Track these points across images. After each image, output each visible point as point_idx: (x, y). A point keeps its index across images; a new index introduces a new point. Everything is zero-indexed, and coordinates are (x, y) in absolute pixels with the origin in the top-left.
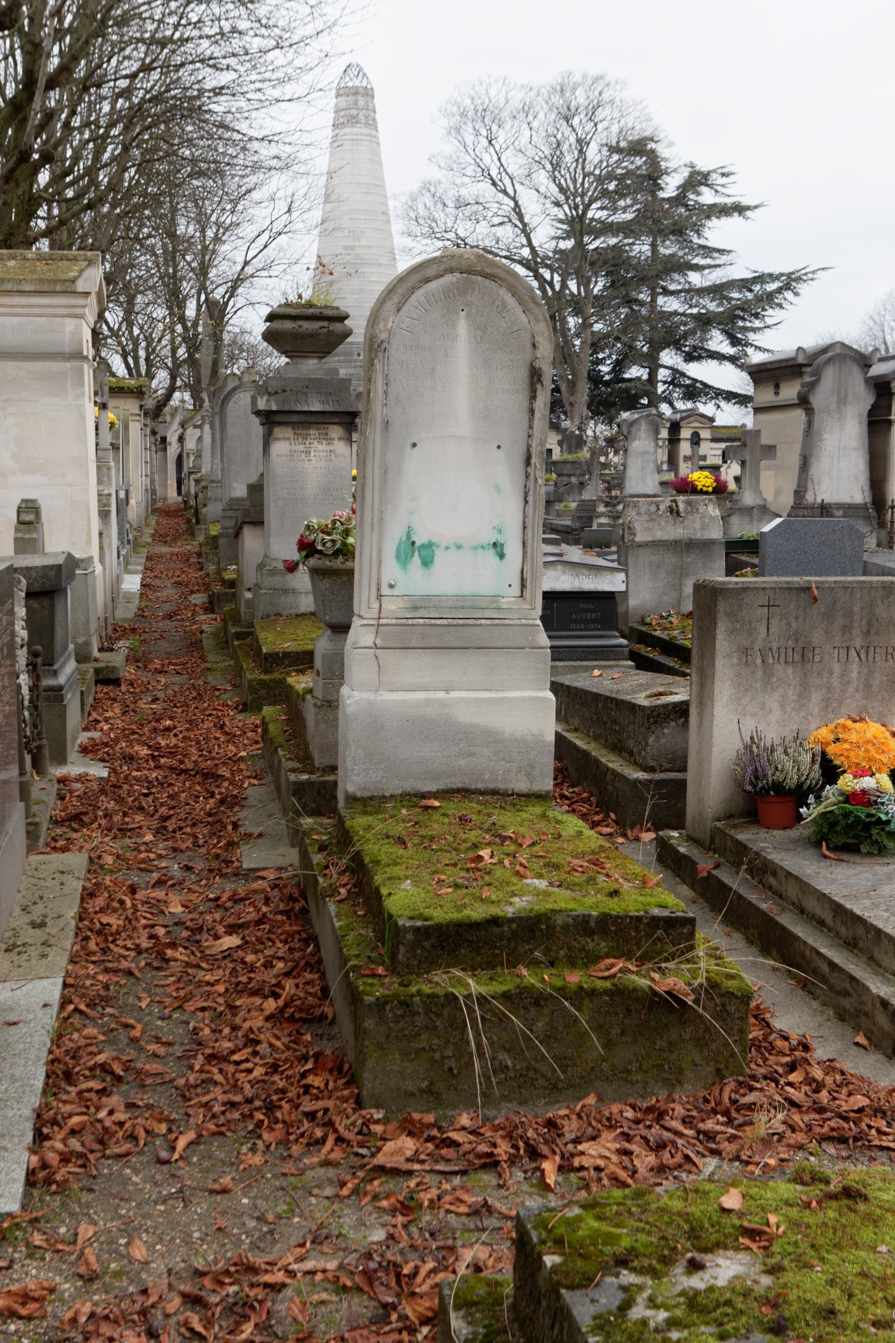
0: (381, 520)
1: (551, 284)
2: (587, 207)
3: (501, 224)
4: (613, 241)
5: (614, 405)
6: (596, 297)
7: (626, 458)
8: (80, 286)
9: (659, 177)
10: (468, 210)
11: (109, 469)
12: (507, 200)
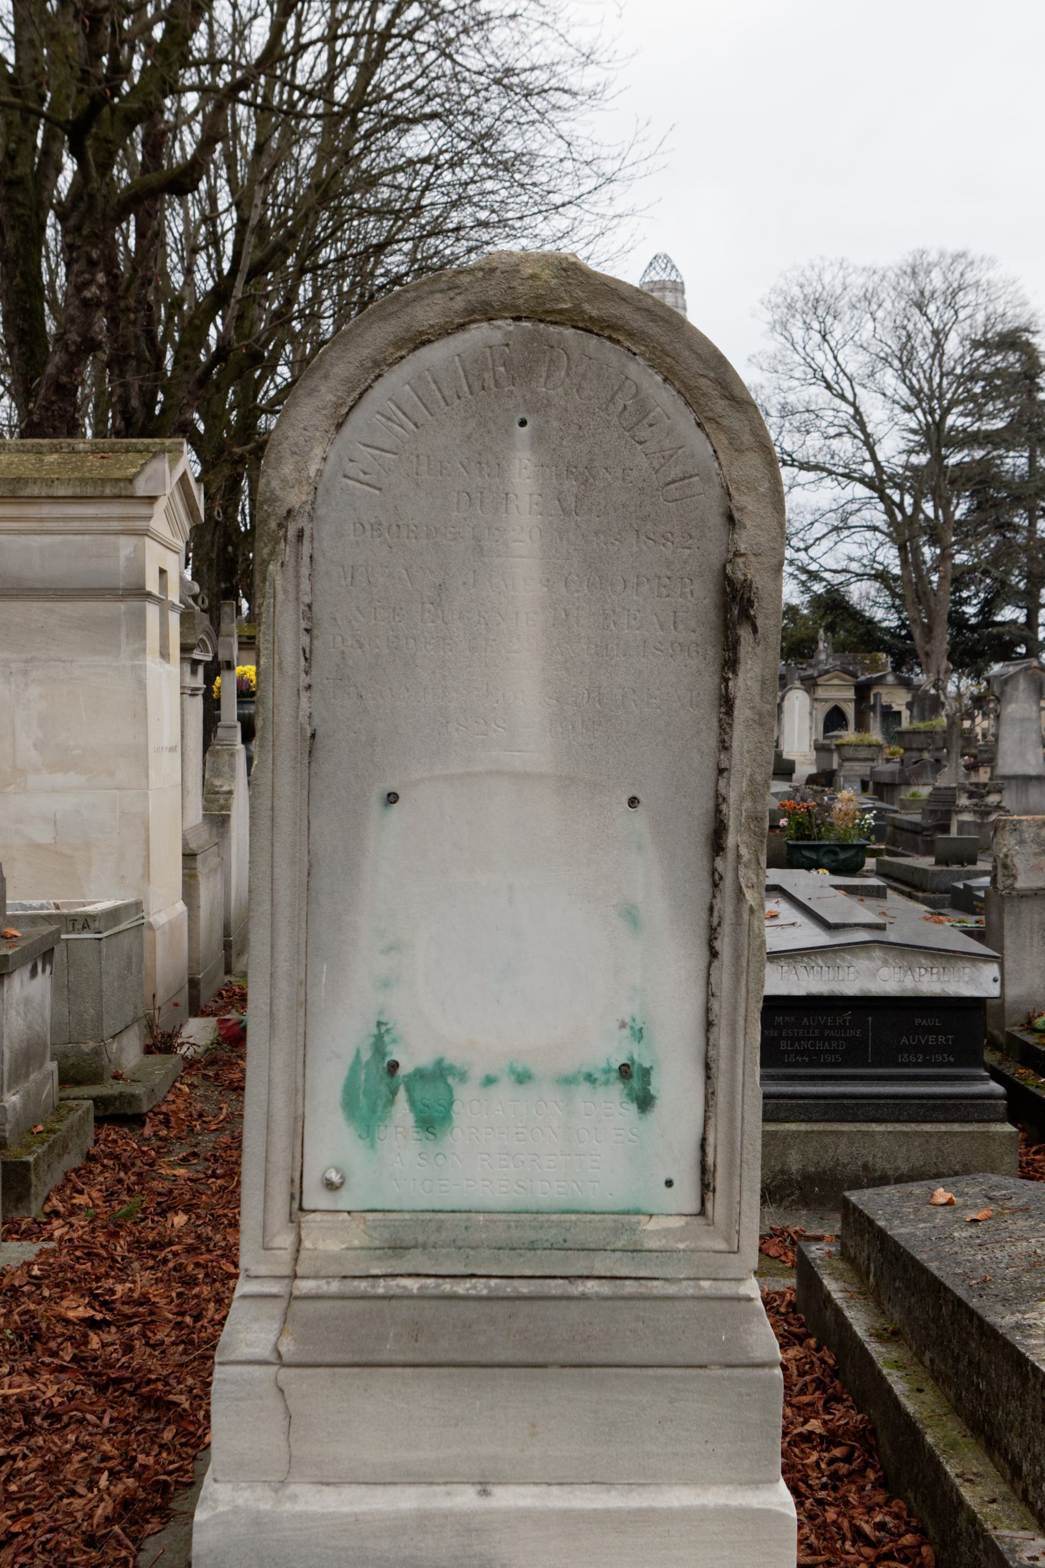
0: (303, 1005)
1: (901, 507)
2: (946, 412)
3: (840, 435)
4: (979, 454)
5: (982, 654)
6: (960, 523)
7: (998, 725)
8: (141, 488)
9: (1037, 375)
10: (797, 420)
11: (232, 755)
12: (845, 406)
